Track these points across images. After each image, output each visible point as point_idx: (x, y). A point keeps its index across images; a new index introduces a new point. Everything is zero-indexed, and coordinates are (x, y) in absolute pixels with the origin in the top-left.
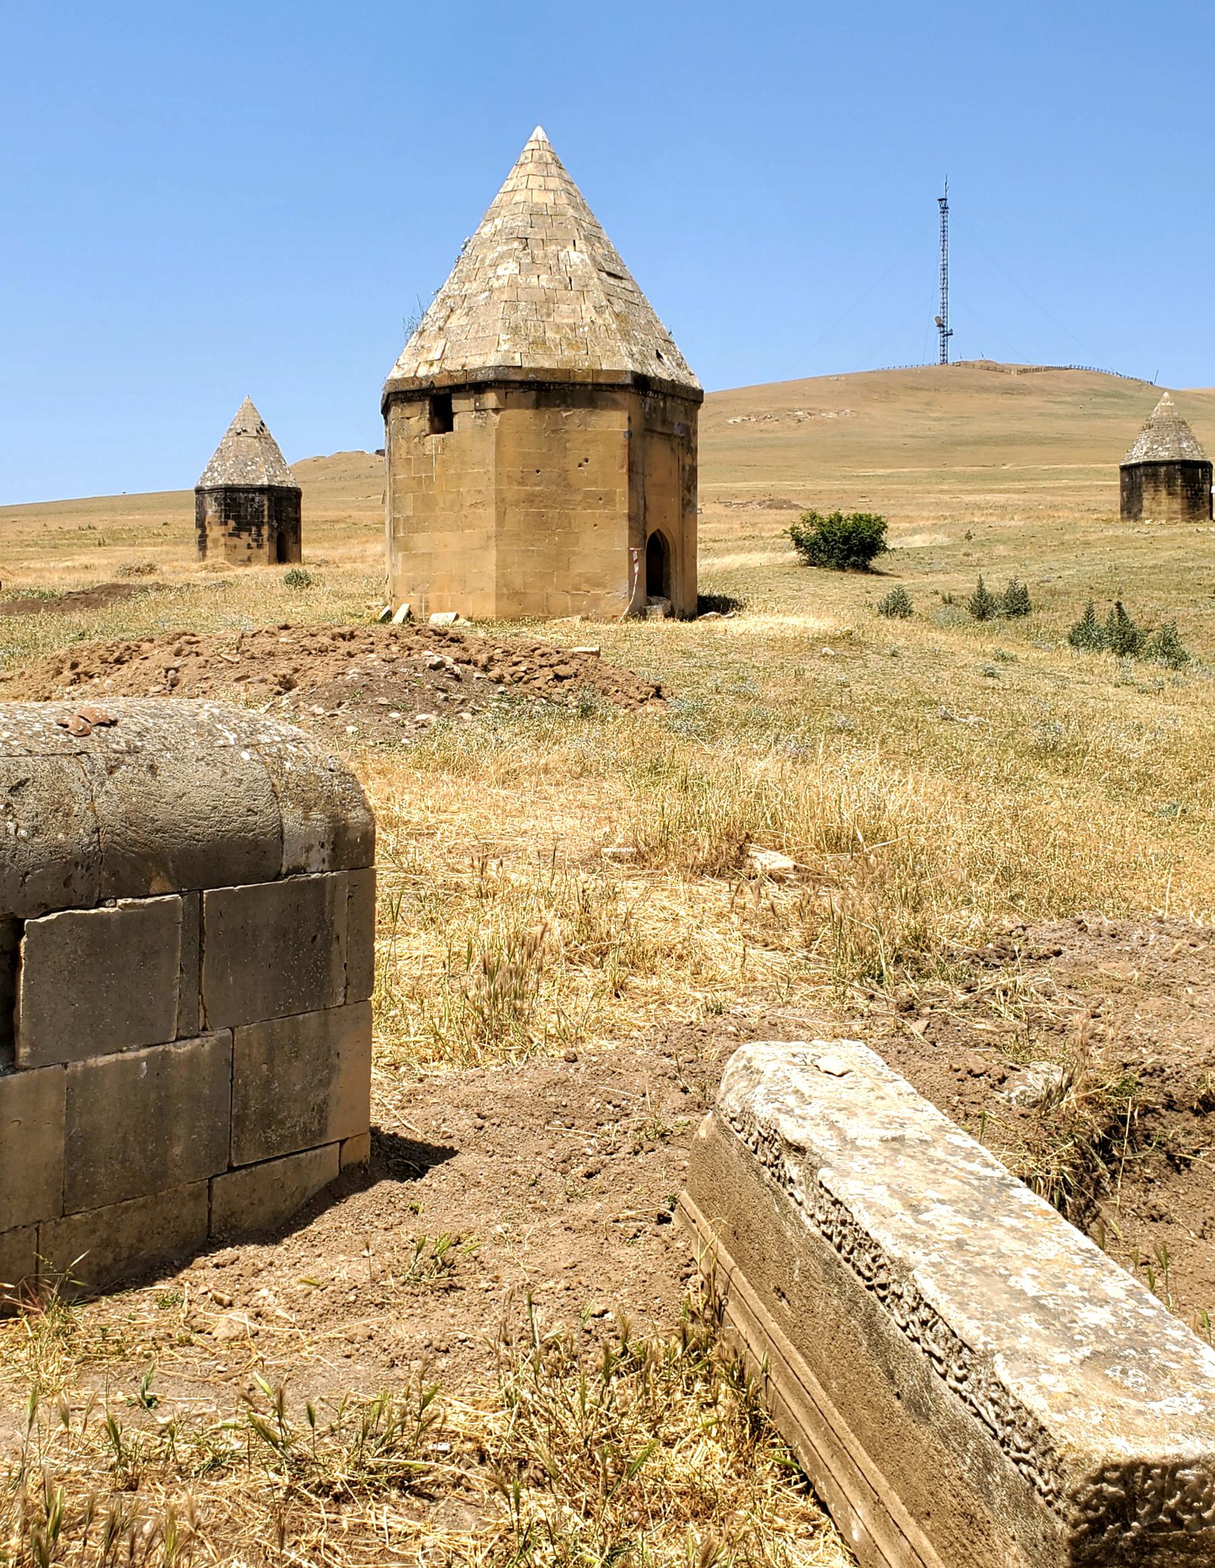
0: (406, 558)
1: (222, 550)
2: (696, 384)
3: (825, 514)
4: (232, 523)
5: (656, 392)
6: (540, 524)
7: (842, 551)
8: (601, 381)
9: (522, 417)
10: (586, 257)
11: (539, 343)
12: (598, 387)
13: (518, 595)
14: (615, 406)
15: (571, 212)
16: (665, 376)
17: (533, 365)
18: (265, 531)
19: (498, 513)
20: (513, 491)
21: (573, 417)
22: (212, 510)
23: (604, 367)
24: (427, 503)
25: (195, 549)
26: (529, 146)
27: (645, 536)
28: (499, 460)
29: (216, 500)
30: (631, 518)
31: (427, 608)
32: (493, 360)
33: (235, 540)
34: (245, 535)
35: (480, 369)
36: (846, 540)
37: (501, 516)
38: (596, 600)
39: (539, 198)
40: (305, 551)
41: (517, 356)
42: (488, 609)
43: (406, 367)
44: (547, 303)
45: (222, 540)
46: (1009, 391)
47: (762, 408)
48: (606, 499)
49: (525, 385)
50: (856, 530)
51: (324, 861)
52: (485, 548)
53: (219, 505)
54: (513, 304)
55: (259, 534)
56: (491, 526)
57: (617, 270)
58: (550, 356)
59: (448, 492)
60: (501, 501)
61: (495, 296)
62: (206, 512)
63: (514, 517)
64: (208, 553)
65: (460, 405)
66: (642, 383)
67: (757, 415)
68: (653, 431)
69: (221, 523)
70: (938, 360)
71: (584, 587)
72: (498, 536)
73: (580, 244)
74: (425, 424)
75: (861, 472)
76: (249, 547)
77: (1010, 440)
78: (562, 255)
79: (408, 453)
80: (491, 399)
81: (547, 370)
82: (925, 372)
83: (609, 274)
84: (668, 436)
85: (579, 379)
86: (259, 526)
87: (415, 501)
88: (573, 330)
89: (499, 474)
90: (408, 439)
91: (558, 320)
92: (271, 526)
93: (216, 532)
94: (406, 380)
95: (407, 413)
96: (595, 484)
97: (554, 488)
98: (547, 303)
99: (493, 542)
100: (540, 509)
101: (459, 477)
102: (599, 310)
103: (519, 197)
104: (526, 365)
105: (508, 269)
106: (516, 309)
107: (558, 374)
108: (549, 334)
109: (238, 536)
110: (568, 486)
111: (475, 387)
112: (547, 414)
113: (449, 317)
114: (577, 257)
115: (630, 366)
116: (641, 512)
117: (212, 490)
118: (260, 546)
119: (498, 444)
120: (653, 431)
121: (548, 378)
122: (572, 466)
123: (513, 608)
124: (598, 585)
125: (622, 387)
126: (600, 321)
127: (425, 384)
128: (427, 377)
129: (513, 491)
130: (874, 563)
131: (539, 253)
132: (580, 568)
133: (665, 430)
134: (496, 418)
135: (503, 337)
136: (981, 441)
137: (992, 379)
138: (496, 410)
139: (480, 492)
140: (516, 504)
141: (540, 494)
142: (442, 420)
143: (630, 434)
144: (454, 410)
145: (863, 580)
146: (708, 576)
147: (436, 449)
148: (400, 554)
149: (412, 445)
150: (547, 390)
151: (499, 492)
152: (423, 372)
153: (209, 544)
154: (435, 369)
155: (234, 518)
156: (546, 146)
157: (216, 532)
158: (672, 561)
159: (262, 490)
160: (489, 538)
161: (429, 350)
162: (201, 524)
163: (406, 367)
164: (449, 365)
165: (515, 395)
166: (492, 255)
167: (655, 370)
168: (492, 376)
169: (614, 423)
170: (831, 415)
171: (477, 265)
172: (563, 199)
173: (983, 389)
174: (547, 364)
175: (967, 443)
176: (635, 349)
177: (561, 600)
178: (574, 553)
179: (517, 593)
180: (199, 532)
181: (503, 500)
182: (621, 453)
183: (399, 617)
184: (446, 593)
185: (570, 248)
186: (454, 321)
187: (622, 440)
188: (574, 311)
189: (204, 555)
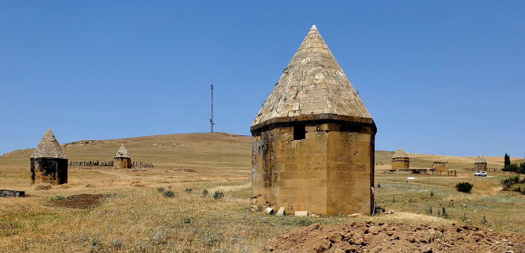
0: (282, 189)
1: (41, 180)
4: (45, 171)
11: (340, 105)
13: (334, 205)
17: (340, 114)
18: (57, 174)
19: (328, 172)
20: (333, 163)
21: (353, 135)
22: (37, 166)
23: (364, 116)
24: (293, 167)
25: (30, 180)
28: (328, 151)
29: (39, 162)
31: (292, 209)
32: (327, 111)
33: (46, 177)
34: (49, 175)
35: (321, 114)
38: (360, 207)
39: (323, 51)
40: (69, 180)
41: (335, 110)
42: (324, 210)
43: (282, 113)
44: (337, 91)
45: (41, 176)
46: (231, 141)
48: (363, 167)
52: (321, 186)
53: (40, 164)
55: (55, 175)
56: (324, 177)
59: (303, 163)
60: (328, 167)
61: (318, 86)
62: (35, 167)
63: (334, 174)
64: (35, 181)
67: (162, 143)
69: (41, 171)
70: (211, 131)
71: (356, 202)
72: (328, 181)
74: (292, 136)
76: (51, 179)
77: (234, 155)
79: (283, 147)
80: (325, 127)
81: (345, 116)
82: (207, 134)
85: (355, 121)
86: (54, 172)
87: (286, 166)
89: (328, 156)
90: (283, 142)
92: (58, 172)
93: (38, 174)
94: (283, 118)
95: (283, 131)
97: (346, 163)
98: (337, 91)
99: (325, 184)
101: (309, 157)
105: (320, 77)
107: (349, 118)
109: (47, 175)
110: (351, 162)
111: (316, 121)
113: (297, 94)
117: (37, 159)
118: (55, 179)
123: (332, 210)
124: (360, 201)
126: (357, 99)
127: (292, 120)
128: (294, 117)
129: (333, 163)
132: (354, 195)
134: (327, 134)
135: (328, 102)
136: (227, 155)
137: (226, 138)
138: (327, 131)
139: (319, 163)
141: (342, 164)
142: (299, 134)
144: (306, 130)
147: (297, 146)
148: (278, 188)
149: (285, 144)
151: (328, 163)
152: (291, 115)
153: (36, 178)
154: (297, 114)
155: (45, 169)
156: (318, 32)
157: (38, 174)
159: (55, 159)
160: (323, 182)
161: (292, 106)
162: (33, 170)
163: (282, 113)
164: (303, 112)
166: (310, 72)
168: (327, 117)
170: (183, 145)
171: (304, 75)
173: (224, 140)
174: (345, 114)
175: (223, 155)
177: (349, 207)
178: (353, 189)
179: (334, 204)
180: (32, 173)
181: (329, 167)
183: (281, 211)
184: (302, 203)
185: (338, 71)
186: (300, 95)
189: (34, 182)
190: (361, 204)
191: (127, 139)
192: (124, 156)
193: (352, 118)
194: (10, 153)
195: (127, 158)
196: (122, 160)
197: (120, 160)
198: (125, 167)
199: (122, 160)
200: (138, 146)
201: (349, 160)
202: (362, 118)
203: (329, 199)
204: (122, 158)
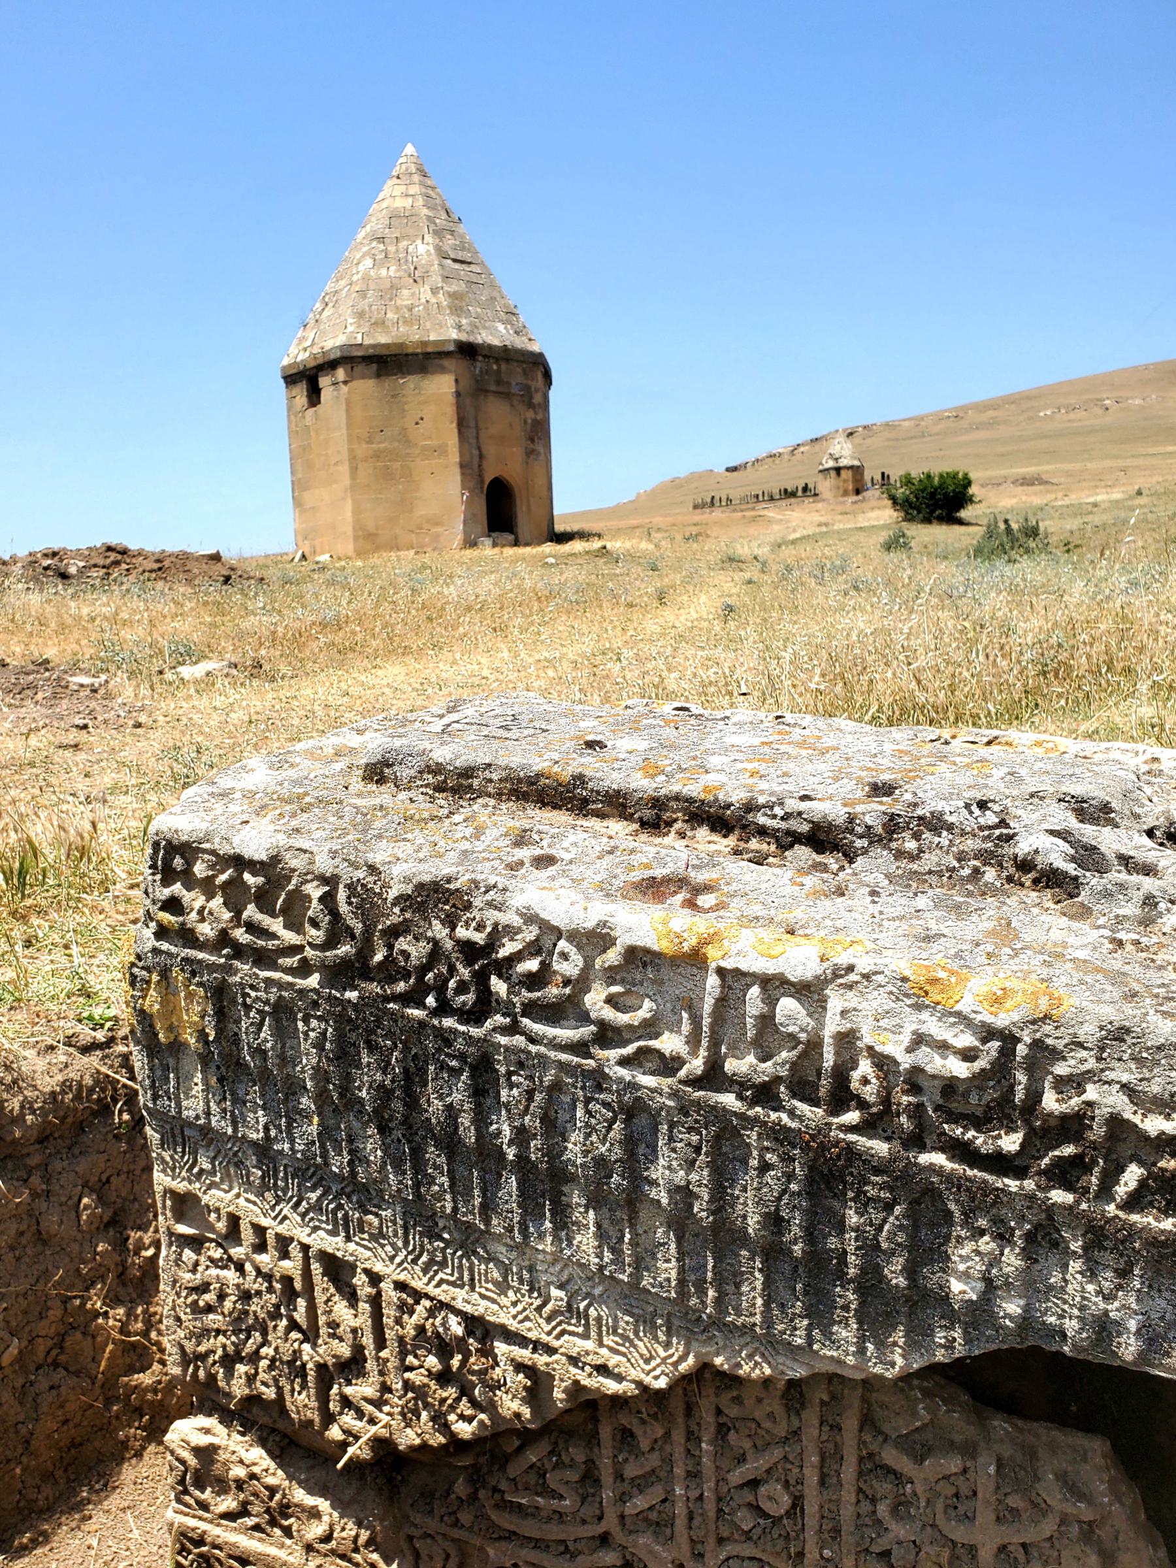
2: (535, 348)
3: (916, 473)
5: (485, 356)
6: (387, 475)
7: (928, 506)
8: (430, 350)
9: (367, 386)
10: (431, 248)
12: (427, 356)
14: (443, 370)
15: (425, 211)
16: (496, 342)
17: (372, 342)
20: (362, 449)
21: (409, 383)
26: (401, 160)
27: (482, 482)
28: (349, 425)
30: (463, 466)
32: (341, 340)
36: (932, 495)
37: (354, 471)
39: (400, 203)
42: (349, 548)
47: (1072, 400)
49: (368, 359)
50: (942, 485)
51: (880, 790)
52: (344, 499)
54: (363, 294)
56: (346, 481)
57: (467, 256)
58: (387, 333)
60: (353, 458)
63: (366, 471)
65: (324, 381)
66: (467, 350)
67: (1067, 407)
68: (487, 391)
71: (426, 526)
73: (428, 238)
75: (1161, 449)
78: (411, 248)
80: (341, 374)
83: (455, 260)
84: (506, 396)
85: (410, 351)
88: (410, 310)
89: (350, 436)
91: (399, 302)
96: (430, 438)
98: (394, 288)
100: (385, 463)
102: (434, 291)
103: (384, 205)
104: (366, 342)
106: (364, 297)
108: (390, 315)
110: (407, 441)
111: (330, 365)
112: (388, 382)
114: (423, 249)
115: (454, 335)
116: (476, 460)
119: (347, 411)
120: (487, 391)
121: (385, 352)
122: (410, 425)
124: (437, 524)
125: (448, 354)
129: (362, 449)
130: (963, 514)
131: (392, 249)
132: (422, 511)
133: (501, 389)
134: (344, 389)
135: (350, 321)
138: (345, 383)
140: (365, 460)
143: (458, 394)
145: (957, 529)
146: (565, 517)
150: (386, 362)
151: (351, 451)
158: (518, 502)
165: (359, 369)
167: (485, 337)
168: (339, 354)
169: (441, 387)
172: (420, 201)
174: (383, 339)
176: (464, 321)
182: (450, 411)
185: (419, 242)
187: (451, 399)
188: (413, 294)
190: (439, 529)
191: (965, 408)
192: (844, 462)
193: (401, 345)
194: (653, 490)
195: (851, 467)
196: (838, 474)
197: (833, 473)
198: (846, 493)
199: (838, 474)
200: (991, 424)
201: (404, 438)
202: (425, 344)
203: (359, 526)
204: (838, 470)
